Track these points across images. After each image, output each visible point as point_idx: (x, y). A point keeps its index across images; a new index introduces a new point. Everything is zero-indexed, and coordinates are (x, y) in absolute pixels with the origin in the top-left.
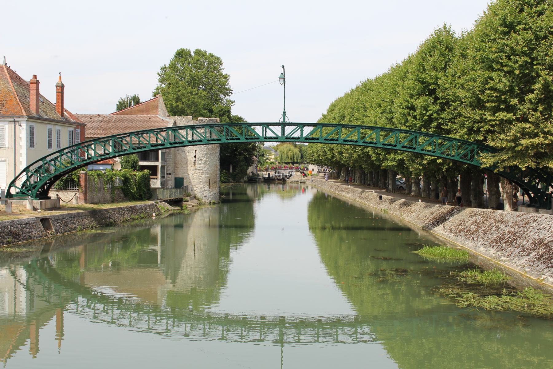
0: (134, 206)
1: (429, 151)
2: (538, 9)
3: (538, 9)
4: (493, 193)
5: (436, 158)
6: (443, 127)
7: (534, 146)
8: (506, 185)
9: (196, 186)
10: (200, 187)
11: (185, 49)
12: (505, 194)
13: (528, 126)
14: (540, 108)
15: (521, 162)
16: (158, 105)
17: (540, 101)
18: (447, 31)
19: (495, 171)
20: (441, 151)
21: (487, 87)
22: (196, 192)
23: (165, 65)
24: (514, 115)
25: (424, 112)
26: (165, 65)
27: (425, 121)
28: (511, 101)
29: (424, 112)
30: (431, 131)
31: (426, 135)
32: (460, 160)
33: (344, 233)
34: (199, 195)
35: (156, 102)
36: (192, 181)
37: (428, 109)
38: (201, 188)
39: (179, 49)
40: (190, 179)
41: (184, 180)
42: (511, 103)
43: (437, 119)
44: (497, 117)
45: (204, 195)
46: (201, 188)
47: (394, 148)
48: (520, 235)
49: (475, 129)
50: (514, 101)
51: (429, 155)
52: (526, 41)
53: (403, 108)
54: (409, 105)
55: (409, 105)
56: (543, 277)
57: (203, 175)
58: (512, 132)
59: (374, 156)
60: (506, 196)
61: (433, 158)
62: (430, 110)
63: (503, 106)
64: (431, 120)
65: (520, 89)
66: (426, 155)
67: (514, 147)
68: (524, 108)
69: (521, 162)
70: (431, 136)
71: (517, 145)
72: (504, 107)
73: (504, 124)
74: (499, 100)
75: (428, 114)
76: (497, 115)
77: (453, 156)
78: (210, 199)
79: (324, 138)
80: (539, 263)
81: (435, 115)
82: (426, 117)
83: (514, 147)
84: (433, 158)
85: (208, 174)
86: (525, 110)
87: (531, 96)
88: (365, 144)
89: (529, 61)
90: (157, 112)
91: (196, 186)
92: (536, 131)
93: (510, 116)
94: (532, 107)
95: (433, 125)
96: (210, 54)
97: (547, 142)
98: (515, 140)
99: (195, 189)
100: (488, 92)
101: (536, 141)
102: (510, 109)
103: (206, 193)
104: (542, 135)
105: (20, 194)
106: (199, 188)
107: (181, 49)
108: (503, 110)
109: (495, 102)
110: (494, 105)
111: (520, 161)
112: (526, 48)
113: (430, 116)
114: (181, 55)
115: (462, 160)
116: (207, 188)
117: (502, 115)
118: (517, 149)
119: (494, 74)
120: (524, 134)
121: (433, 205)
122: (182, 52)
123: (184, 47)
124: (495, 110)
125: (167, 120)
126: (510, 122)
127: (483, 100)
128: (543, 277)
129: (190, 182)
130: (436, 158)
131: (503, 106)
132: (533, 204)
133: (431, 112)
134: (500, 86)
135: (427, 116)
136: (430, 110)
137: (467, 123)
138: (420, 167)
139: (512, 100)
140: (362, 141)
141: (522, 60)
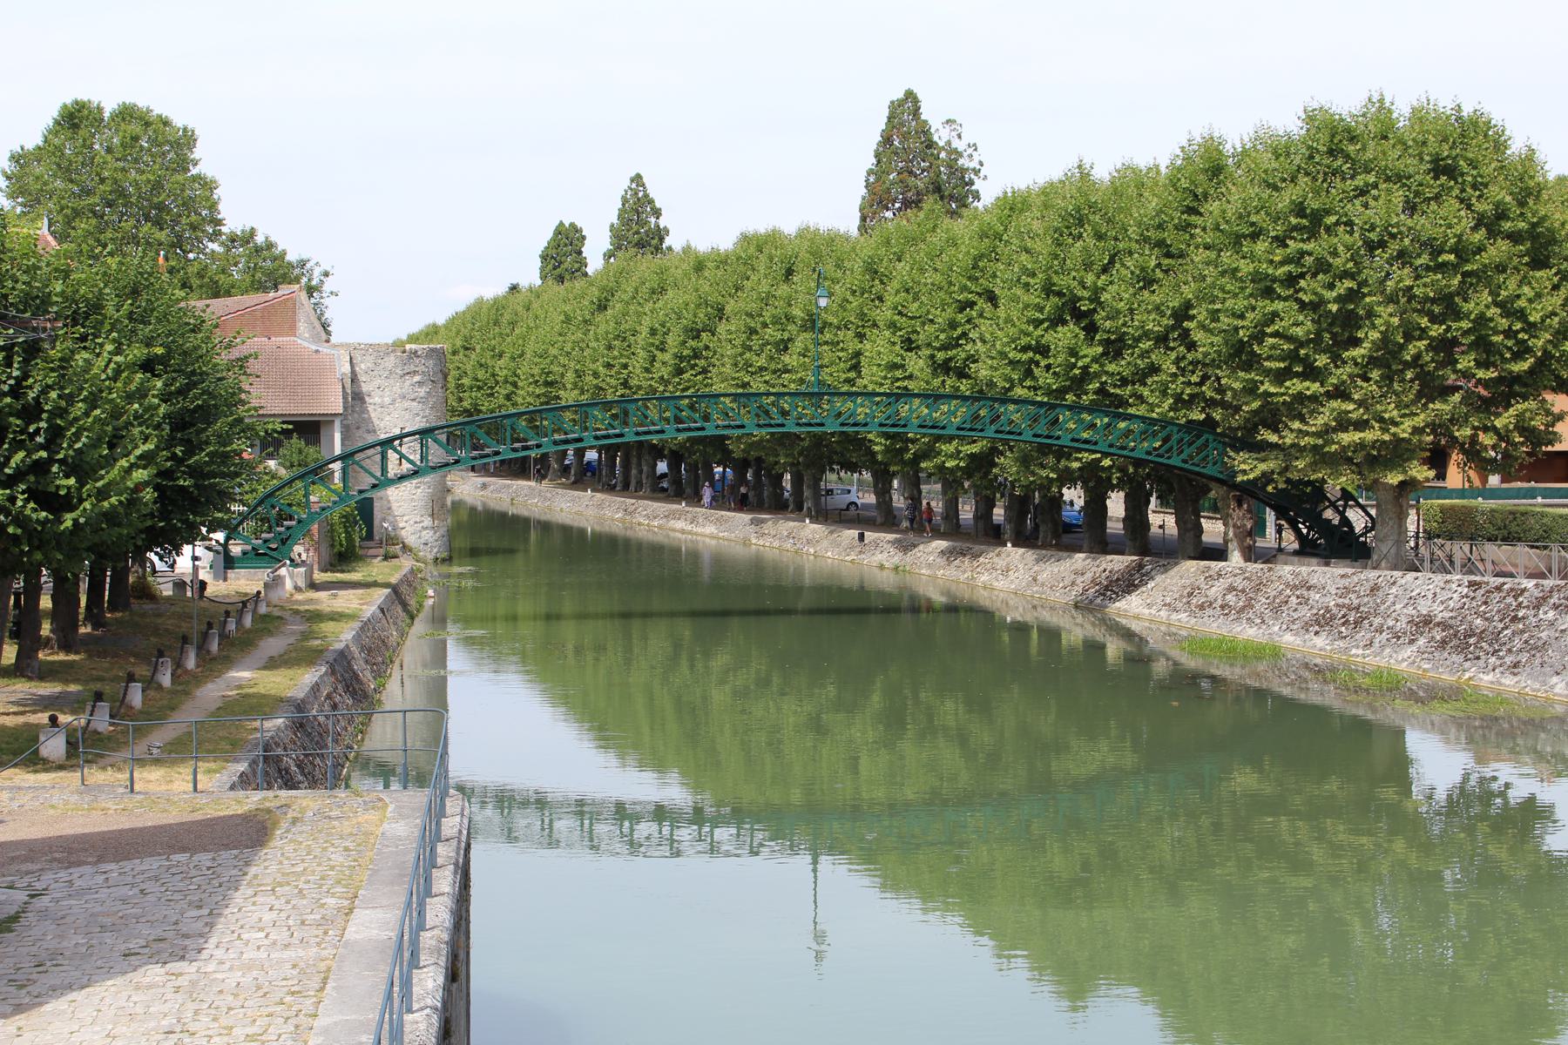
0: (326, 571)
1: (1086, 442)
2: (1356, 182)
3: (1356, 182)
4: (1189, 526)
5: (1099, 455)
6: (1112, 391)
7: (1361, 446)
8: (1234, 510)
9: (405, 519)
10: (414, 520)
11: (86, 100)
12: (1231, 530)
13: (1351, 407)
14: (1375, 374)
15: (1332, 474)
16: (294, 312)
17: (1372, 361)
18: (1084, 174)
19: (1270, 489)
20: (1108, 442)
21: (1268, 330)
22: (403, 533)
23: (22, 149)
24: (1322, 386)
25: (1073, 360)
26: (22, 149)
27: (1074, 379)
28: (1316, 360)
29: (1073, 360)
30: (1086, 399)
31: (1075, 408)
32: (1183, 465)
33: (685, 629)
34: (411, 540)
35: (289, 304)
36: (394, 506)
37: (1081, 354)
38: (416, 522)
39: (69, 101)
40: (389, 501)
41: (375, 504)
42: (1317, 364)
43: (1097, 375)
44: (1287, 388)
45: (423, 541)
46: (416, 522)
47: (1056, 442)
48: (1372, 611)
49: (1187, 398)
50: (1322, 360)
51: (1086, 450)
52: (1349, 250)
53: (1015, 349)
54: (1033, 342)
55: (1033, 342)
56: (1467, 675)
57: (419, 490)
58: (1320, 421)
59: (881, 443)
60: (1235, 534)
61: (1094, 456)
62: (1085, 356)
63: (1299, 369)
64: (1086, 375)
65: (1334, 336)
66: (1079, 450)
67: (1323, 446)
68: (1342, 374)
69: (1332, 474)
70: (1090, 409)
71: (1328, 442)
72: (1300, 369)
73: (1300, 406)
74: (1293, 357)
75: (1080, 364)
76: (1288, 384)
77: (1133, 450)
78: (435, 550)
79: (955, 426)
80: (1446, 654)
81: (1095, 367)
82: (1077, 372)
83: (1323, 446)
84: (1094, 456)
85: (429, 488)
86: (1345, 377)
87: (1357, 352)
88: (1076, 445)
89: (1355, 287)
90: (292, 330)
91: (405, 519)
92: (1365, 417)
93: (1314, 387)
94: (1356, 371)
95: (1091, 387)
96: (160, 116)
97: (1387, 437)
98: (1326, 431)
99: (401, 525)
100: (1271, 340)
101: (1369, 436)
102: (1311, 373)
103: (428, 535)
104: (1377, 425)
105: (252, 555)
106: (412, 522)
107: (77, 102)
108: (1297, 375)
109: (1283, 359)
110: (1282, 365)
111: (1329, 471)
112: (1351, 265)
113: (1085, 368)
114: (75, 118)
115: (1186, 466)
116: (428, 522)
117: (1296, 386)
118: (1327, 449)
119: (1279, 306)
120: (1343, 424)
121: (1065, 554)
122: (79, 111)
123: (83, 96)
124: (1280, 377)
125: (325, 350)
126: (1314, 398)
127: (1260, 354)
128: (1467, 675)
129: (389, 508)
130: (1099, 455)
131: (1299, 369)
132: (1308, 550)
133: (1088, 360)
134: (1299, 331)
135: (1079, 368)
136: (1085, 356)
137: (1174, 386)
138: (1051, 475)
139: (1317, 357)
140: (1031, 433)
141: (1345, 286)
